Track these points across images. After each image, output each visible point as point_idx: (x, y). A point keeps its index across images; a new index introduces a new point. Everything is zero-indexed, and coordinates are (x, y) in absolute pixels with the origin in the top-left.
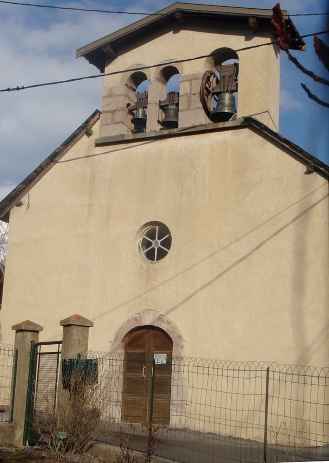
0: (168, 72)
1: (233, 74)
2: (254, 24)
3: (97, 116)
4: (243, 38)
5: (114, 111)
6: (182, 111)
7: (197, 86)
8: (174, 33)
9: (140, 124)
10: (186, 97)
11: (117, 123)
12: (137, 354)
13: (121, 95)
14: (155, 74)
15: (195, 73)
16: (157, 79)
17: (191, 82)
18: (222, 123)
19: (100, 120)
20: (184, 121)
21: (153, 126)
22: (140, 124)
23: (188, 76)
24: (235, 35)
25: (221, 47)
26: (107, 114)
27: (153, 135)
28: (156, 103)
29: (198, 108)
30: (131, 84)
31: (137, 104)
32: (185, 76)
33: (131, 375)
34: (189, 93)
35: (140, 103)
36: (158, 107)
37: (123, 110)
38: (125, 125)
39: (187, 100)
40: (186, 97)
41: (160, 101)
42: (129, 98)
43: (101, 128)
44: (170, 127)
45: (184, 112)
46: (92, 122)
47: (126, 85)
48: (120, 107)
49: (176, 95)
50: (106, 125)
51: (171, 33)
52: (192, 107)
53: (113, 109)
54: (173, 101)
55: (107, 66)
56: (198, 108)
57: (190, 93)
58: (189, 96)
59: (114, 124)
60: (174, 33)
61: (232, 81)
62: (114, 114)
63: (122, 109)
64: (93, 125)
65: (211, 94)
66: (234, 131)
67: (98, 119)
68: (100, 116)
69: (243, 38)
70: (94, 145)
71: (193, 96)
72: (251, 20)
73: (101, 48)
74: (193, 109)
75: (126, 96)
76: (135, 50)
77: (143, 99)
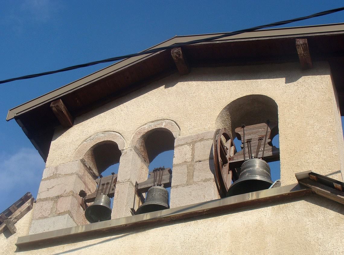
0: (157, 142)
1: (266, 136)
2: (304, 50)
3: (27, 205)
4: (284, 79)
5: (58, 197)
6: (177, 187)
7: (204, 151)
8: (165, 88)
9: (97, 212)
10: (185, 167)
11: (59, 214)
12: (223, 153)
13: (72, 174)
14: (132, 141)
15: (200, 133)
16: (135, 148)
17: (194, 145)
18: (254, 193)
19: (29, 213)
20: (179, 199)
21: (122, 209)
22: (97, 212)
23: (189, 137)
24: (269, 77)
25: (245, 95)
26: (44, 203)
27: (123, 222)
28: (131, 182)
29: (206, 180)
30: (90, 164)
31: (97, 191)
32: (184, 138)
33: (13, 211)
34: (190, 160)
35: (102, 190)
36: (133, 191)
37: (73, 195)
38: (74, 220)
39: (186, 170)
40: (185, 167)
41: (136, 183)
42: (85, 183)
43: (30, 223)
44: (153, 212)
45: (180, 188)
46: (17, 213)
47: (83, 161)
48: (68, 191)
49: (166, 172)
50: (40, 218)
51: (163, 87)
52: (195, 179)
53: (56, 195)
54: (160, 180)
55: (53, 141)
56: (206, 180)
57: (192, 160)
58: (190, 165)
59: (54, 216)
60: (165, 88)
61: (265, 145)
62: (56, 202)
63: (72, 193)
64: (18, 218)
65: (228, 165)
66: (276, 207)
67: (29, 209)
68: (32, 204)
69: (284, 79)
70: (15, 247)
71: (197, 163)
72: (300, 42)
73: (50, 103)
74: (196, 183)
75: (80, 177)
76: (102, 114)
77: (108, 184)
